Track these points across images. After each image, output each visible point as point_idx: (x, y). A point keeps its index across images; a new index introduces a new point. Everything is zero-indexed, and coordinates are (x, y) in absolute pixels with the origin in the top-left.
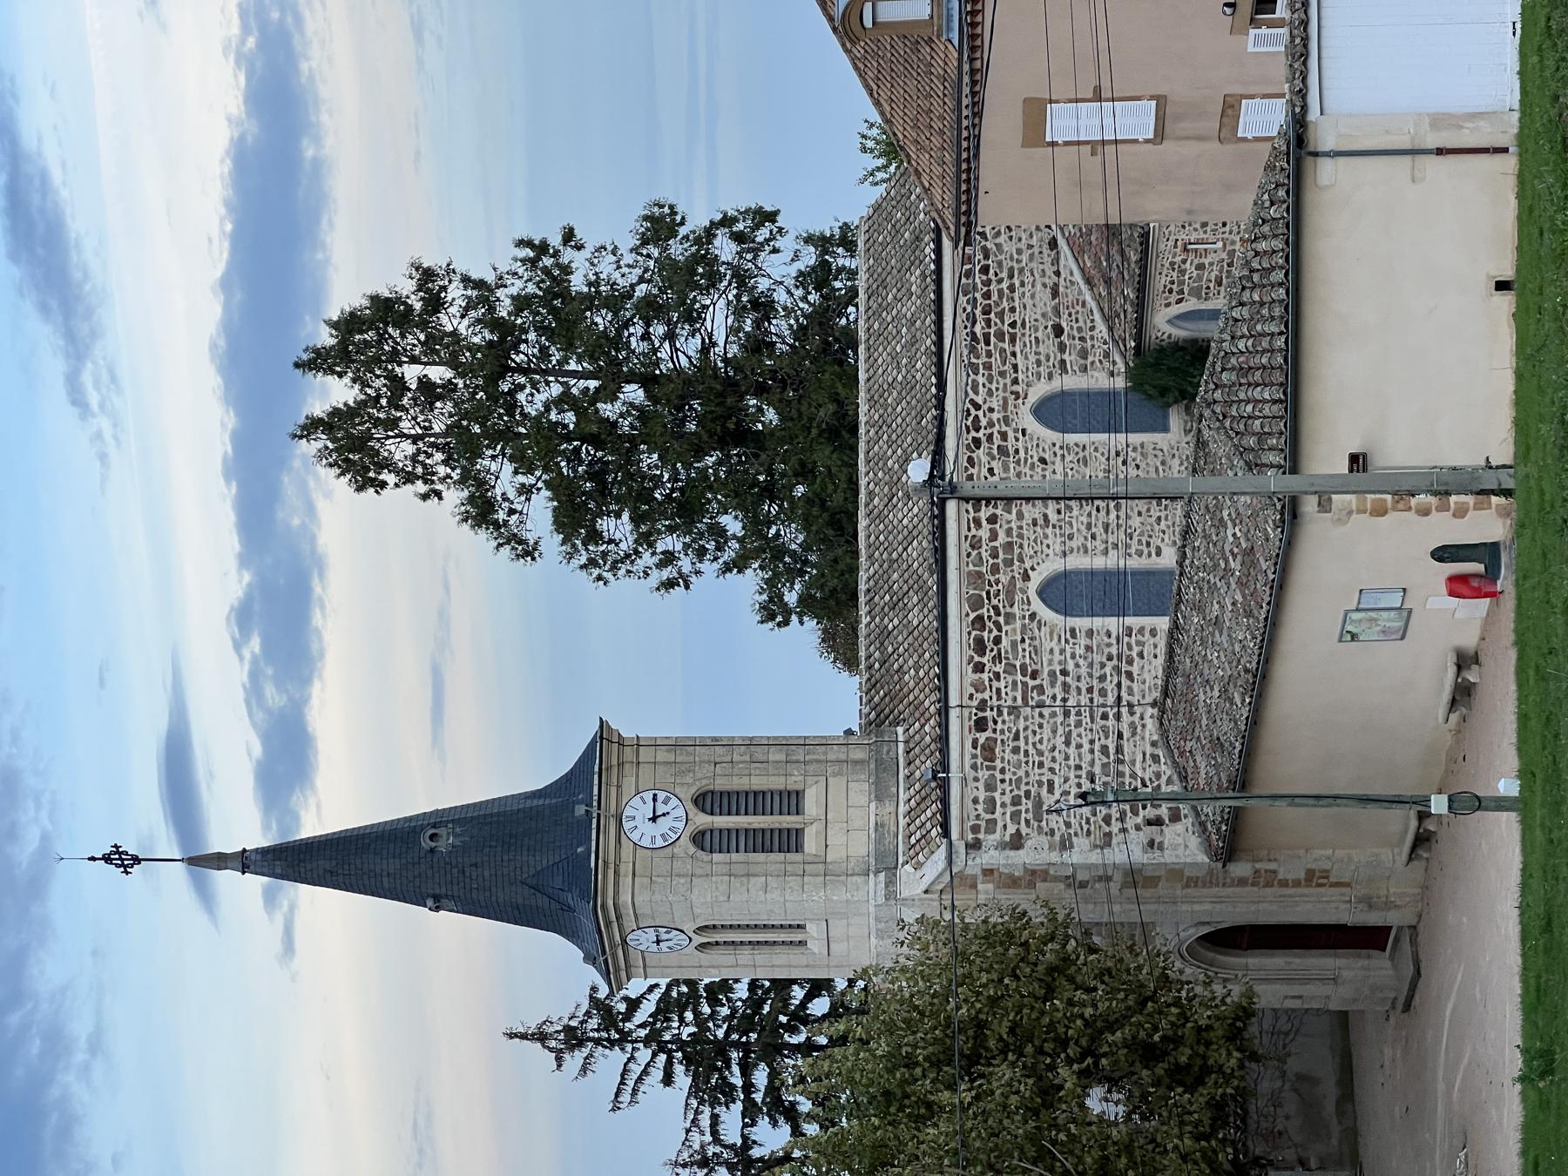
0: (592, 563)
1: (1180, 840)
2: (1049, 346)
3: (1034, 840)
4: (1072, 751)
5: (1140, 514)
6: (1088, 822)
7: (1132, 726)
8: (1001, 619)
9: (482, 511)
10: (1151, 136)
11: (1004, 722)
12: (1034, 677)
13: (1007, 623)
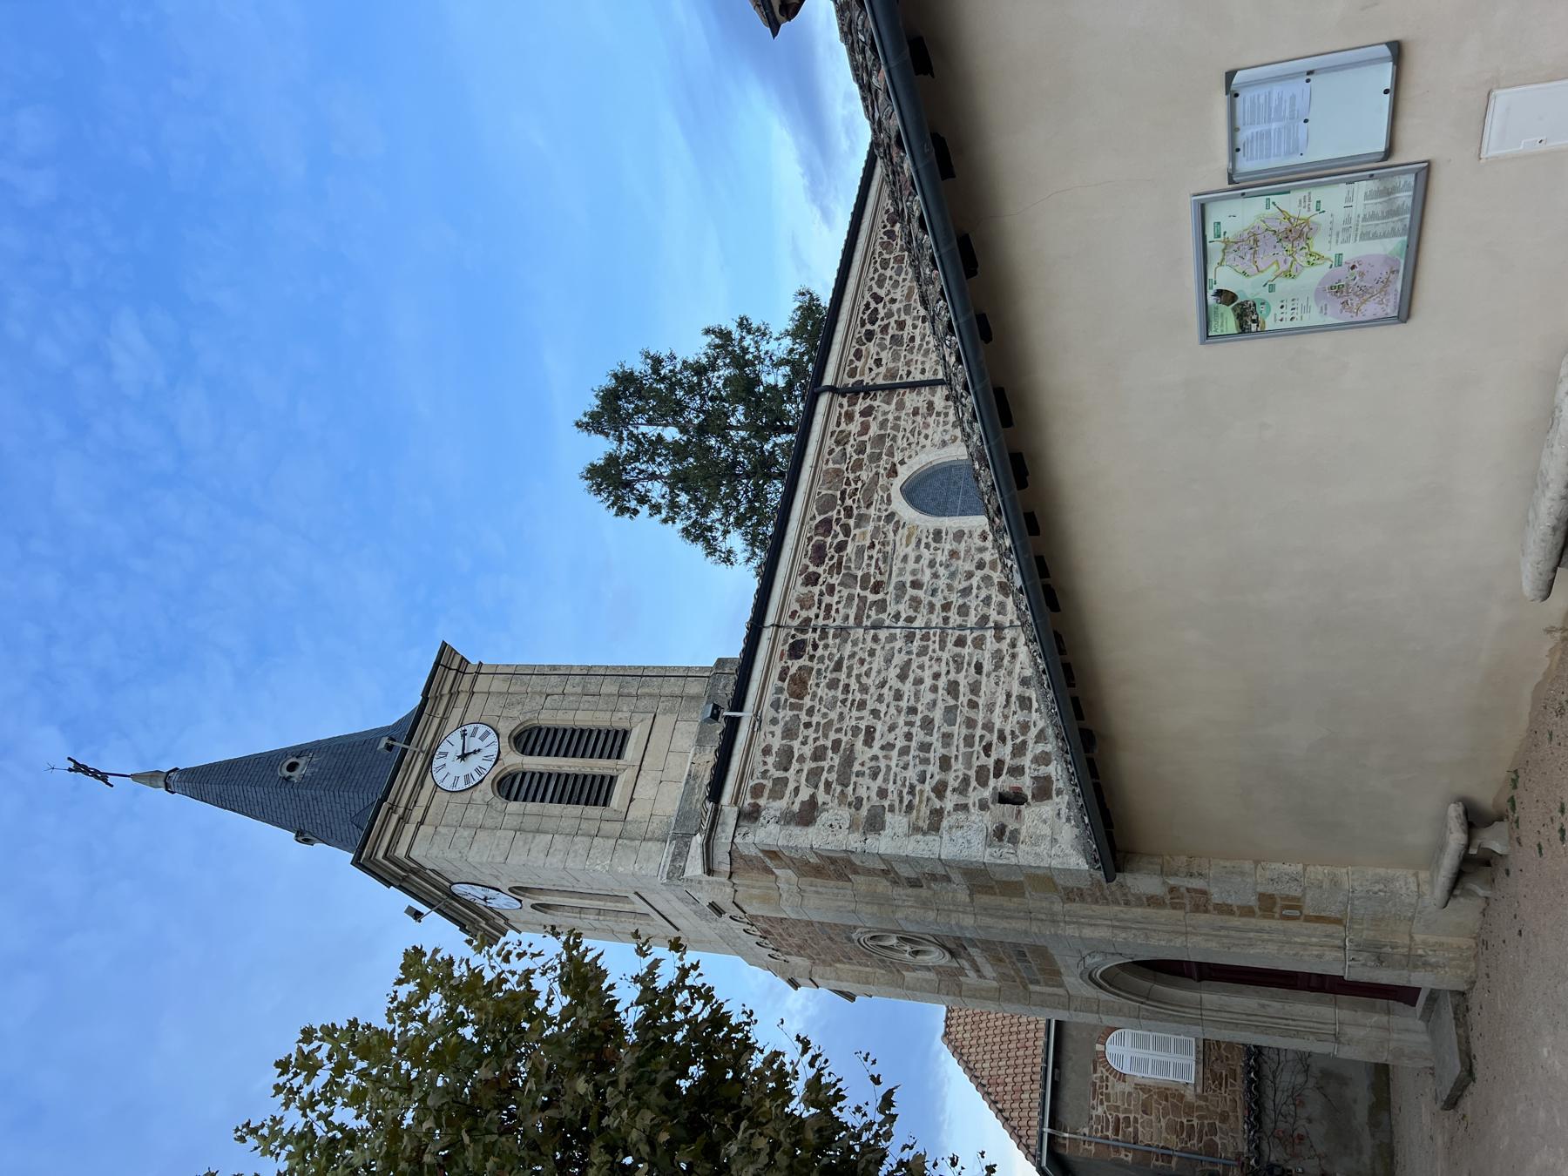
3: (834, 814)
4: (907, 688)
6: (912, 791)
7: (998, 657)
8: (852, 522)
11: (826, 647)
12: (877, 588)
13: (857, 526)
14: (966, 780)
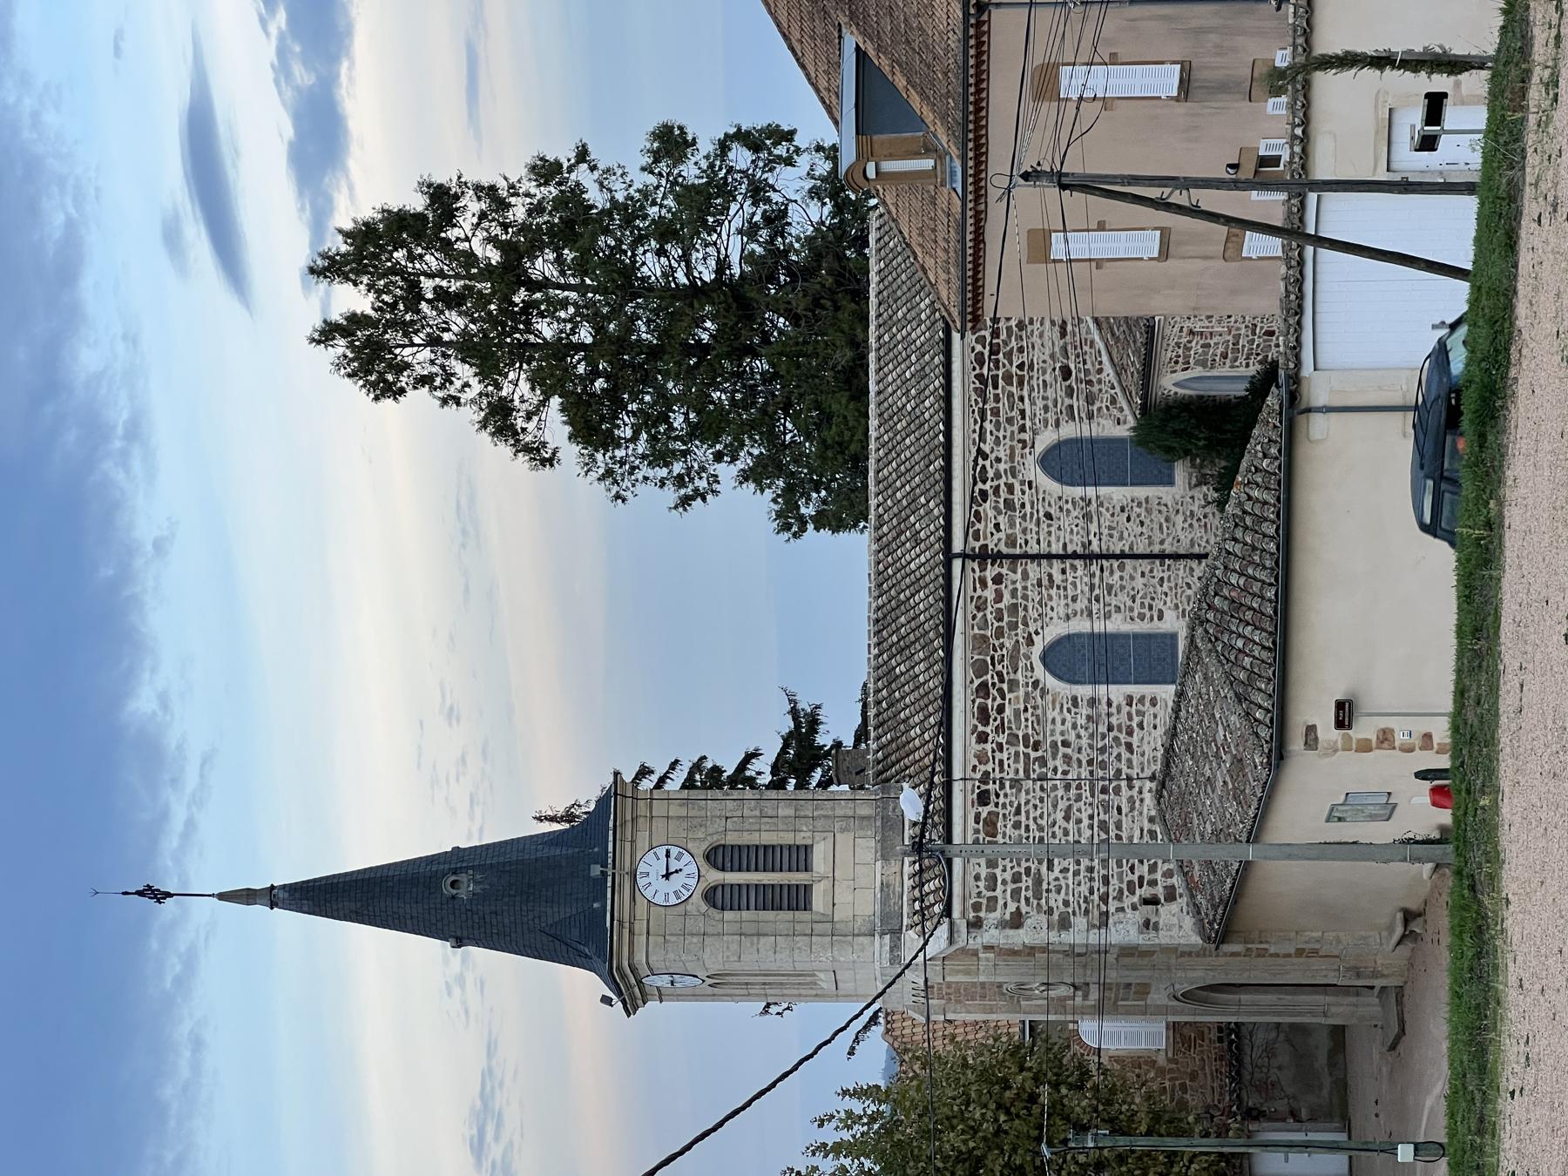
0: (609, 473)
1: (1175, 921)
2: (1057, 391)
3: (1035, 919)
4: (1071, 826)
5: (1143, 574)
7: (1131, 800)
8: (1005, 686)
9: (499, 418)
10: (1156, 255)
11: (1006, 795)
13: (1010, 691)
14: (1121, 891)
